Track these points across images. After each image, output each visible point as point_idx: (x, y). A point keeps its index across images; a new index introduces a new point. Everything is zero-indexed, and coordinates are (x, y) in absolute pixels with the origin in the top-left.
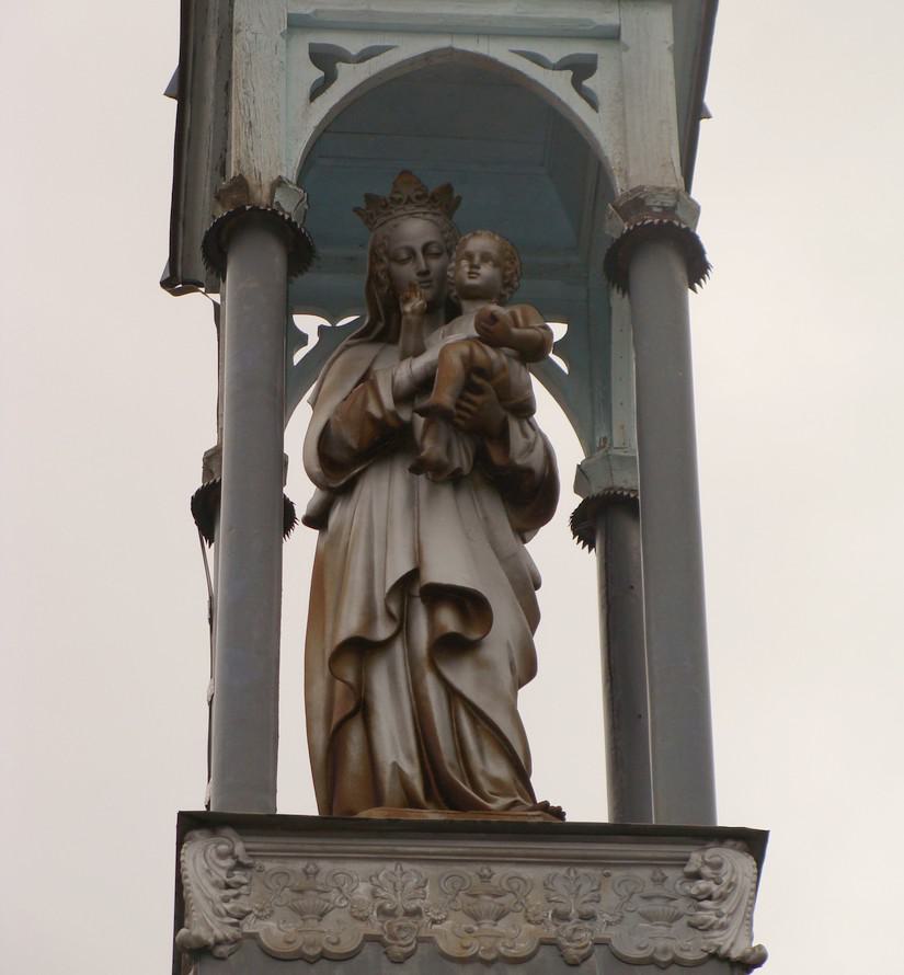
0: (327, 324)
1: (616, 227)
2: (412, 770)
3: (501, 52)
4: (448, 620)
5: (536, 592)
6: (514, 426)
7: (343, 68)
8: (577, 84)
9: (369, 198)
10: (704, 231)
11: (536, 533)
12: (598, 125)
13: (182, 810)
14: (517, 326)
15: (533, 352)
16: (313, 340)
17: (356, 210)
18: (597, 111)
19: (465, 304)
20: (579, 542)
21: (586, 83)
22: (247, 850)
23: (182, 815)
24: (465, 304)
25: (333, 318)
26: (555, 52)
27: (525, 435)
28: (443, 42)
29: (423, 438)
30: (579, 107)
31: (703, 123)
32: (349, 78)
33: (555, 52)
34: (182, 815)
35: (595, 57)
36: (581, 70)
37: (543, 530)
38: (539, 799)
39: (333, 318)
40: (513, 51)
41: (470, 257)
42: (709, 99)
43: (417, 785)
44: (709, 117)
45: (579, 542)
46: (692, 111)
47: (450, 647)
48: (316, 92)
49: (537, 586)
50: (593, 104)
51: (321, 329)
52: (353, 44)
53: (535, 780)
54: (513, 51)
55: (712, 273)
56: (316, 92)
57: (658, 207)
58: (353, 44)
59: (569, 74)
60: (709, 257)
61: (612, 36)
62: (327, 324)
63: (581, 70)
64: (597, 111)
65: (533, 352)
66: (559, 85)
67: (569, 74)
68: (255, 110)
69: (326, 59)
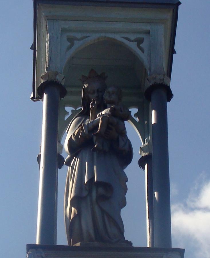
0: (74, 109)
1: (148, 84)
2: (92, 231)
3: (118, 37)
4: (101, 190)
5: (126, 183)
6: (120, 139)
7: (76, 42)
8: (138, 46)
9: (83, 76)
10: (172, 87)
11: (127, 167)
12: (143, 57)
13: (28, 244)
14: (121, 111)
15: (128, 117)
16: (70, 113)
17: (80, 80)
18: (144, 53)
19: (108, 105)
20: (141, 168)
21: (141, 45)
22: (45, 255)
23: (27, 245)
24: (108, 105)
25: (76, 108)
26: (132, 37)
27: (123, 140)
28: (103, 35)
29: (96, 142)
30: (139, 52)
31: (174, 55)
32: (77, 45)
33: (132, 37)
34: (27, 245)
35: (143, 39)
36: (139, 42)
37: (129, 166)
38: (126, 239)
39: (76, 108)
40: (122, 37)
41: (109, 93)
42: (176, 48)
43: (93, 235)
44: (176, 53)
45: (141, 168)
46: (172, 51)
47: (102, 198)
48: (70, 47)
49: (127, 181)
50: (143, 51)
51: (72, 111)
52: (79, 36)
53: (125, 234)
54: (122, 37)
55: (174, 97)
56: (70, 47)
57: (159, 79)
58: (79, 36)
59: (136, 43)
60: (173, 93)
61: (148, 33)
62: (74, 109)
63: (139, 42)
64: (144, 53)
65: (128, 117)
66: (133, 46)
67: (136, 43)
68: (52, 55)
69: (71, 40)
